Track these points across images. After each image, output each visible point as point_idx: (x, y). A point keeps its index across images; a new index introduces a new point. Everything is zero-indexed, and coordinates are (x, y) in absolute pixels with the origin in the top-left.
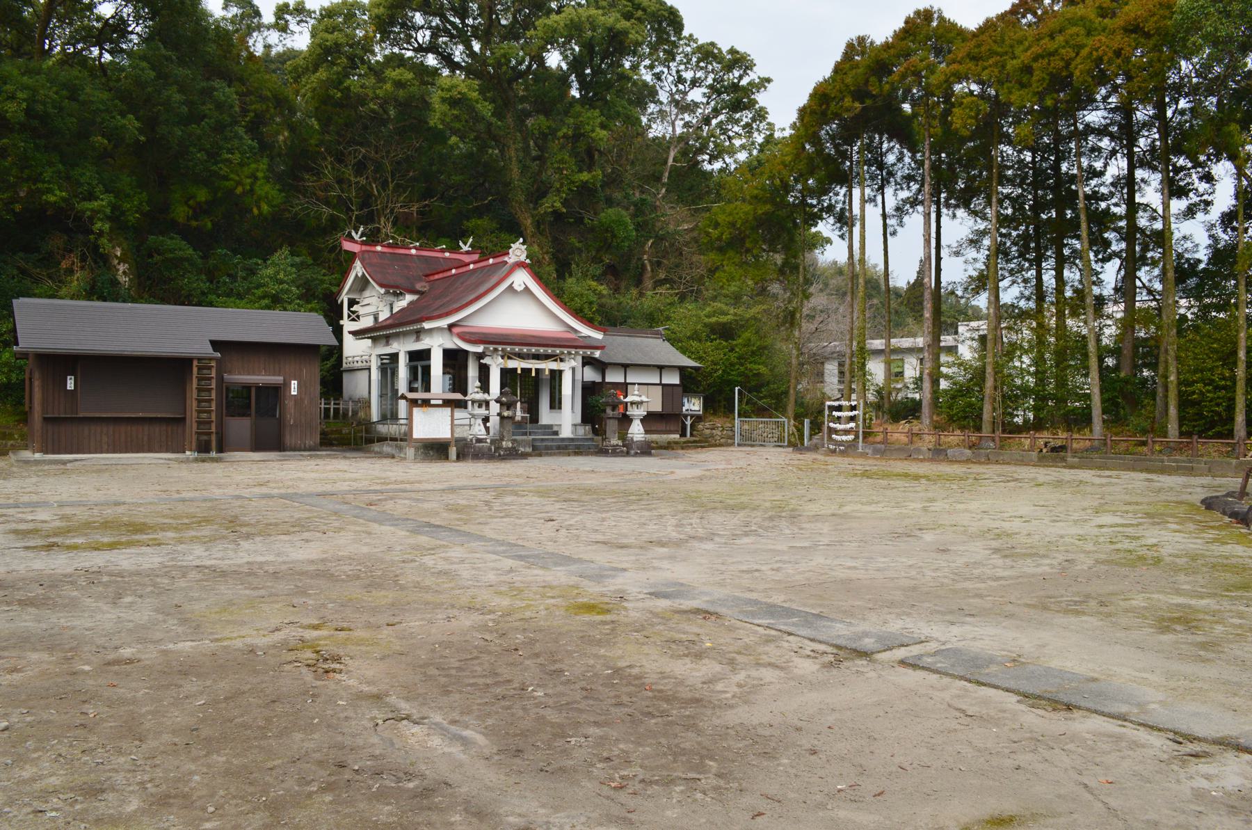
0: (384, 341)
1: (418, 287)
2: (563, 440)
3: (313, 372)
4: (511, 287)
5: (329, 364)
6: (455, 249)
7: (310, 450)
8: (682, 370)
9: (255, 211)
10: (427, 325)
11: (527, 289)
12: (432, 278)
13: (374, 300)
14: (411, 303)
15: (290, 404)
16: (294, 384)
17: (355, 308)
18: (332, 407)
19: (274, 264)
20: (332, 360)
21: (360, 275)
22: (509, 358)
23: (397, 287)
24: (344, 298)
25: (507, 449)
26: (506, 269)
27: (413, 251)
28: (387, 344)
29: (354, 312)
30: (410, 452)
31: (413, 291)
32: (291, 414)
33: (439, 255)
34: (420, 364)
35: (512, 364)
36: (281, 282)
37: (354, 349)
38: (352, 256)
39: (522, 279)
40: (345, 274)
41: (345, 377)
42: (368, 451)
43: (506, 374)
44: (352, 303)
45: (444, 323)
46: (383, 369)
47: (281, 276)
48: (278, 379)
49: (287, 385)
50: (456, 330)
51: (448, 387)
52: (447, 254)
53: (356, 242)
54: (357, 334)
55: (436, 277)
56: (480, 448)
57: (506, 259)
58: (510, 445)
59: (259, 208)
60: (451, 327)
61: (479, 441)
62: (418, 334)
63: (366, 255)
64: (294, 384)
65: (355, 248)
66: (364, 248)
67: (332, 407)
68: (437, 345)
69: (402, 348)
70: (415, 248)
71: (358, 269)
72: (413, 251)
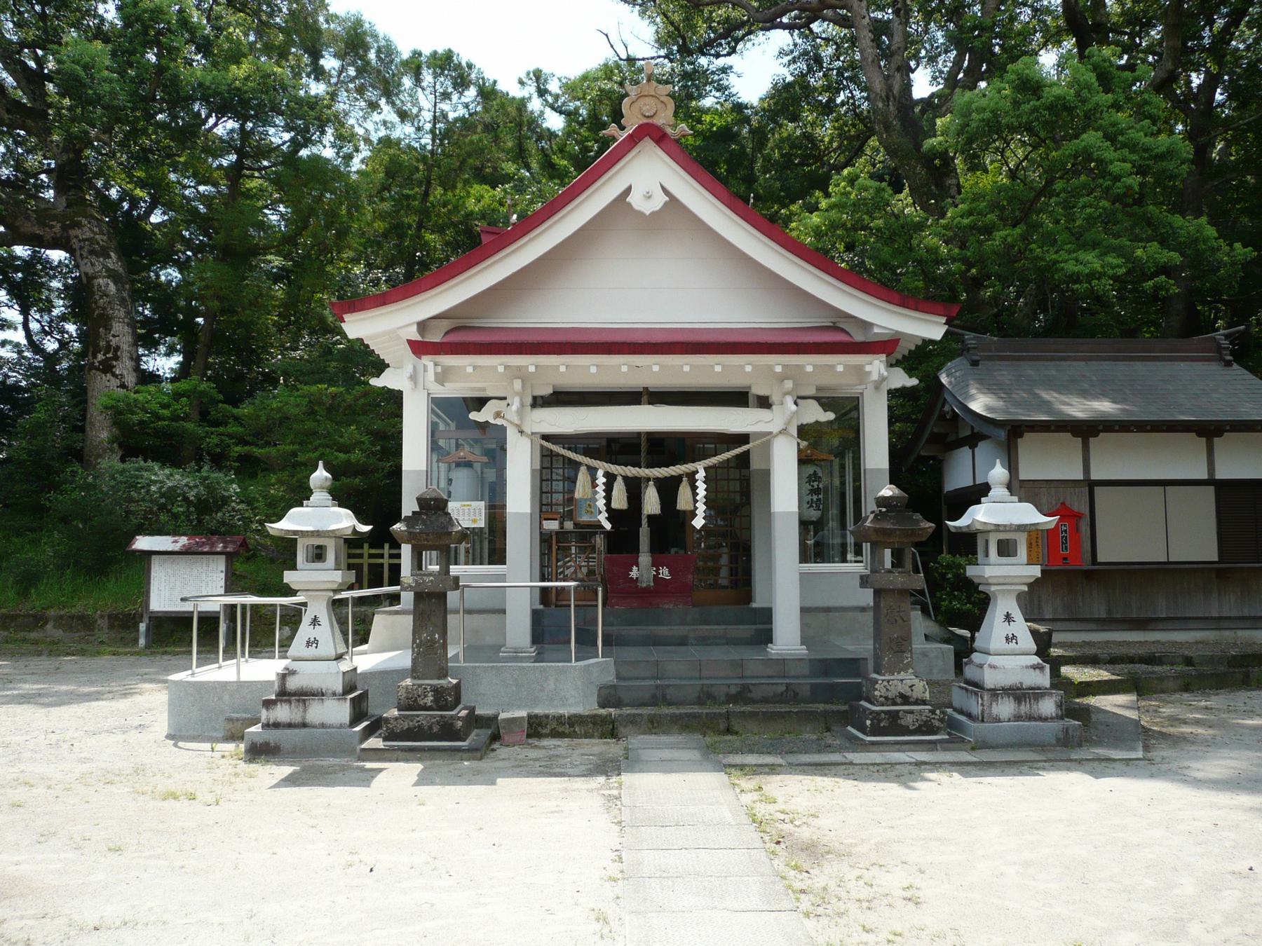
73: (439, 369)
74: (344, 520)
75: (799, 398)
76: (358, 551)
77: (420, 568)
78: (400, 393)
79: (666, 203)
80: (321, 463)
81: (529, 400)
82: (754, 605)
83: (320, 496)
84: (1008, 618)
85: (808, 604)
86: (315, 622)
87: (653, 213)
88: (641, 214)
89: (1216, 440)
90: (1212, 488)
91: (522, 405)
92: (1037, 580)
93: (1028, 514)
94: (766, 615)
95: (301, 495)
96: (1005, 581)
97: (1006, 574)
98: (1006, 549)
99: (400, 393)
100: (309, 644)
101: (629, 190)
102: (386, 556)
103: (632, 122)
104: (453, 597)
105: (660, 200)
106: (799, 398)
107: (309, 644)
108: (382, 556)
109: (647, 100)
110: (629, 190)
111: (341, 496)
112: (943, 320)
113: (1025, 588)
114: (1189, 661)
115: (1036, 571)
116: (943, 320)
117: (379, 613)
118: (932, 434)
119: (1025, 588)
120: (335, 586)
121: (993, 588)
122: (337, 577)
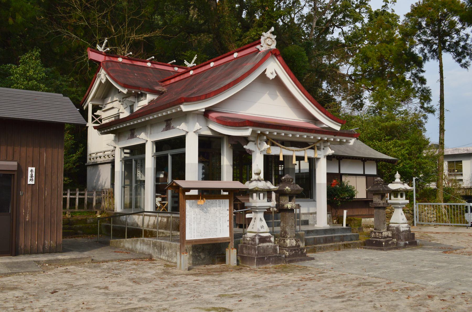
0: (129, 134)
1: (158, 88)
2: (317, 232)
3: (56, 158)
4: (263, 75)
5: (75, 157)
6: (180, 63)
7: (52, 251)
8: (377, 161)
9: (11, 21)
10: (185, 108)
11: (277, 80)
12: (168, 83)
13: (116, 104)
14: (151, 102)
15: (26, 199)
16: (31, 171)
17: (98, 113)
18: (77, 197)
19: (24, 63)
20: (78, 153)
21: (103, 81)
22: (273, 145)
23: (139, 88)
24: (89, 105)
25: (291, 248)
26: (258, 57)
27: (149, 64)
28: (133, 136)
29: (97, 116)
30: (183, 260)
31: (153, 92)
32: (27, 208)
33: (170, 69)
34: (170, 153)
35: (275, 151)
36: (31, 79)
37: (99, 144)
38: (95, 66)
39: (274, 68)
40: (88, 84)
41: (89, 170)
42: (117, 249)
43: (269, 160)
44: (95, 108)
45: (201, 106)
46: (127, 163)
47: (31, 72)
48: (12, 165)
49: (21, 173)
50: (213, 115)
51: (201, 176)
52: (176, 69)
53: (100, 53)
54: (103, 129)
55: (173, 81)
56: (265, 249)
57: (258, 47)
58: (294, 243)
59: (14, 18)
60: (208, 112)
61: (263, 240)
62: (168, 123)
63: (110, 64)
64: (31, 171)
65: (101, 58)
66: (107, 58)
67: (77, 197)
68: (192, 133)
69: (148, 139)
70: (151, 61)
71: (103, 76)
72: (149, 64)
76: (71, 197)
87: (273, 79)
88: (268, 79)
102: (69, 194)
105: (275, 75)
108: (71, 194)
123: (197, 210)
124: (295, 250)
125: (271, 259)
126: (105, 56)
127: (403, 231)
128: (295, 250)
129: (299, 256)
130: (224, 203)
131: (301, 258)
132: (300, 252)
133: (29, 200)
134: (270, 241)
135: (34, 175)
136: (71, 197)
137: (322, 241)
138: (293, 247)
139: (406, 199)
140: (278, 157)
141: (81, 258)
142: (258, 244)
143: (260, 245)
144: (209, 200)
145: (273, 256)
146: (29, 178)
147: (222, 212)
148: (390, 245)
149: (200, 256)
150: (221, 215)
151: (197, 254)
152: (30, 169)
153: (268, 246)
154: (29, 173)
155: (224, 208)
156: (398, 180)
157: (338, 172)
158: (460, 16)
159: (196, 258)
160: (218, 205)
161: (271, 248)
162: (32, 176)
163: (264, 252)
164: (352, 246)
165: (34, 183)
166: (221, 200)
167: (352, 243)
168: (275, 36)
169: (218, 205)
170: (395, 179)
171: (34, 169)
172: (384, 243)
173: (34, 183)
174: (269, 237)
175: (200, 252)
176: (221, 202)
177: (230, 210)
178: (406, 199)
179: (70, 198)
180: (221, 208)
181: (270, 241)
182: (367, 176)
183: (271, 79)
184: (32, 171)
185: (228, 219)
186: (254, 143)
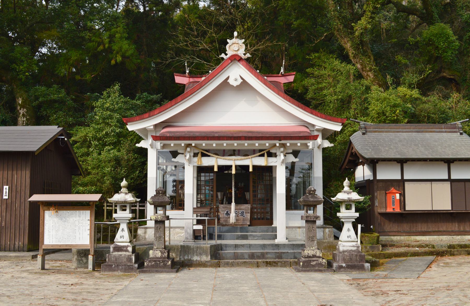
4: (226, 82)
35: (206, 162)
66: (192, 80)
73: (162, 145)
74: (130, 198)
75: (287, 153)
76: (141, 208)
77: (156, 213)
78: (146, 150)
79: (242, 82)
80: (124, 179)
81: (192, 154)
82: (273, 226)
83: (123, 190)
84: (349, 230)
85: (287, 226)
86: (123, 230)
87: (237, 86)
88: (233, 86)
89: (451, 164)
90: (449, 182)
91: (190, 156)
92: (358, 217)
93: (355, 196)
94: (275, 229)
95: (117, 190)
96: (123, 219)
97: (347, 215)
98: (348, 208)
99: (146, 150)
100: (121, 237)
101: (228, 78)
102: (138, 206)
103: (230, 52)
104: (167, 223)
105: (240, 81)
106: (287, 153)
107: (121, 237)
108: (140, 206)
109: (235, 45)
110: (228, 78)
111: (130, 189)
112: (341, 124)
113: (354, 220)
114: (433, 247)
115: (357, 215)
116: (341, 124)
117: (140, 228)
118: (349, 160)
119: (354, 220)
120: (129, 219)
121: (343, 220)
122: (130, 216)
123: (56, 220)
124: (154, 261)
125: (120, 267)
126: (189, 77)
127: (344, 251)
128: (154, 261)
129: (160, 267)
130: (84, 213)
131: (157, 269)
132: (162, 264)
133: (5, 211)
134: (127, 251)
135: (7, 192)
136: (141, 208)
137: (246, 256)
138: (157, 258)
139: (356, 211)
140: (212, 167)
141: (24, 256)
142: (113, 252)
143: (114, 253)
144: (68, 211)
145: (123, 265)
146: (4, 194)
147: (81, 222)
148: (313, 266)
149: (82, 260)
150: (81, 224)
151: (80, 259)
152: (5, 187)
153: (121, 255)
154: (5, 190)
155: (84, 218)
156: (346, 188)
157: (399, 178)
158: (199, 10)
159: (80, 262)
160: (77, 215)
161: (124, 257)
162: (6, 193)
163: (116, 260)
164: (279, 264)
165: (7, 198)
166: (81, 211)
167: (279, 262)
168: (243, 40)
169: (77, 215)
170: (343, 187)
171: (7, 187)
172: (301, 264)
173: (7, 198)
174: (127, 247)
175: (82, 257)
176: (81, 213)
177: (91, 221)
178: (356, 211)
179: (139, 210)
180: (81, 218)
181: (127, 251)
182: (452, 181)
183: (235, 86)
184: (6, 188)
185: (89, 228)
186: (183, 155)
